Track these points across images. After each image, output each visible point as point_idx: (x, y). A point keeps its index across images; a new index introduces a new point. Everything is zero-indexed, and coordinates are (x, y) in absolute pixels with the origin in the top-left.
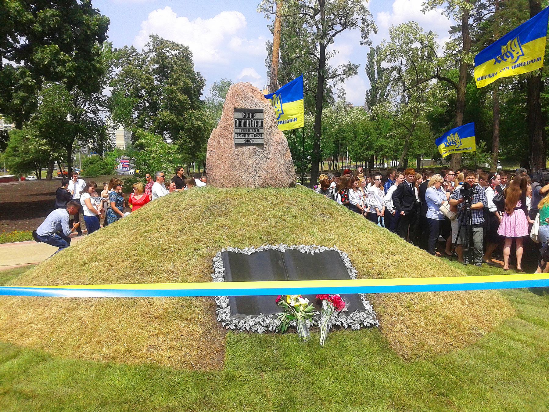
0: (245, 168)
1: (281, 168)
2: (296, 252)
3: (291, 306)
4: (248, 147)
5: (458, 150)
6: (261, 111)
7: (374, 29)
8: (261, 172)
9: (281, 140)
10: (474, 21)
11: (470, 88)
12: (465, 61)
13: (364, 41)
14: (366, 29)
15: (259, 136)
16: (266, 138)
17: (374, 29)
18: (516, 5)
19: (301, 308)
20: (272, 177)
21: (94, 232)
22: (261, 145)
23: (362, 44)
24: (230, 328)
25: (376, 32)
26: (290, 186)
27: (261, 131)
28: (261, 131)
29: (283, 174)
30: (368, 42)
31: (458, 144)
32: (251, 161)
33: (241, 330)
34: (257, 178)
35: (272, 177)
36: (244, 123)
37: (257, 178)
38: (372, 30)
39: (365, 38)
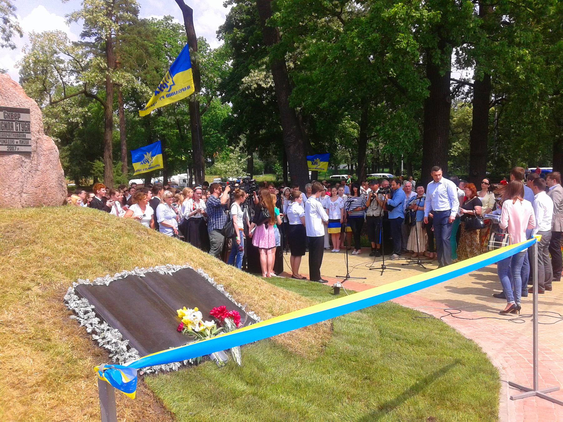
0: (8, 183)
1: (54, 183)
2: (157, 274)
3: (197, 332)
4: (11, 156)
5: (151, 168)
6: (27, 111)
7: (19, 31)
8: (29, 188)
9: (51, 149)
10: (96, 39)
11: (92, 108)
12: (114, 80)
13: (5, 43)
14: (8, 31)
15: (26, 142)
16: (34, 145)
17: (19, 31)
18: (135, 31)
19: (208, 332)
20: (45, 194)
21: (188, 245)
22: (27, 154)
23: (3, 46)
24: (145, 373)
25: (21, 36)
26: (63, 205)
27: (28, 136)
28: (28, 136)
29: (56, 189)
30: (10, 46)
31: (150, 162)
32: (16, 174)
33: (157, 373)
34: (24, 195)
35: (45, 194)
36: (6, 126)
37: (24, 195)
38: (16, 32)
39: (7, 39)
